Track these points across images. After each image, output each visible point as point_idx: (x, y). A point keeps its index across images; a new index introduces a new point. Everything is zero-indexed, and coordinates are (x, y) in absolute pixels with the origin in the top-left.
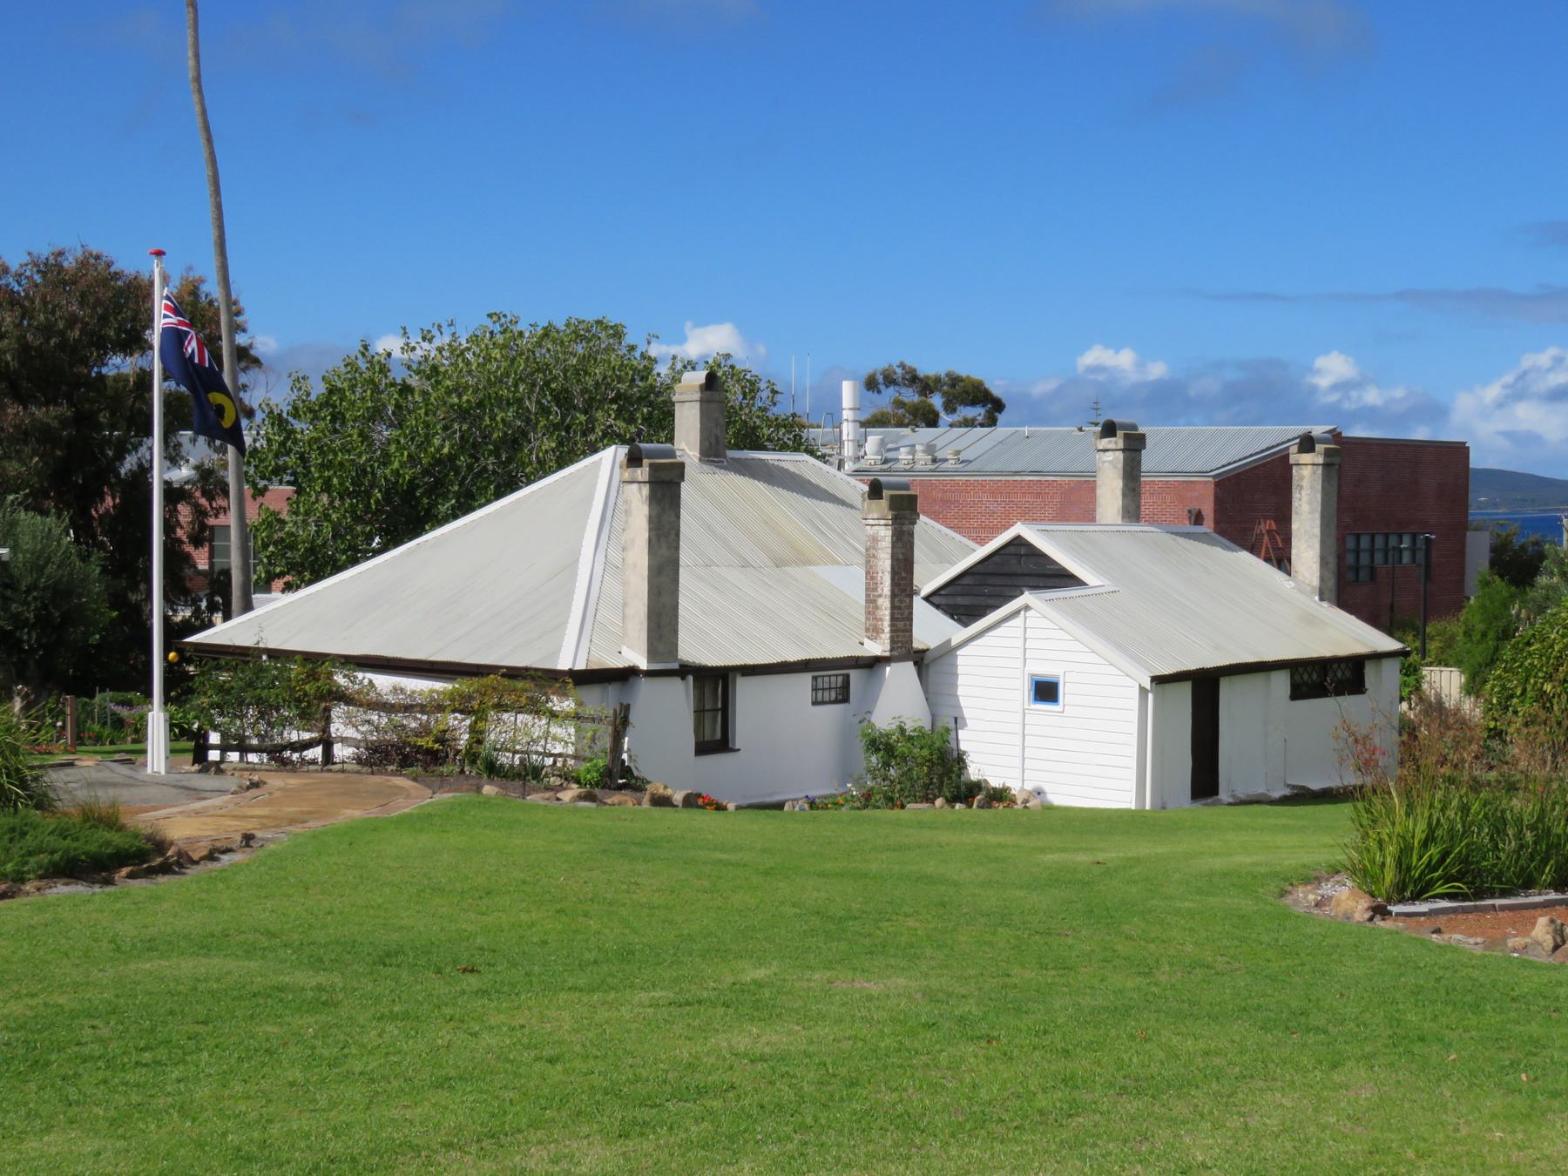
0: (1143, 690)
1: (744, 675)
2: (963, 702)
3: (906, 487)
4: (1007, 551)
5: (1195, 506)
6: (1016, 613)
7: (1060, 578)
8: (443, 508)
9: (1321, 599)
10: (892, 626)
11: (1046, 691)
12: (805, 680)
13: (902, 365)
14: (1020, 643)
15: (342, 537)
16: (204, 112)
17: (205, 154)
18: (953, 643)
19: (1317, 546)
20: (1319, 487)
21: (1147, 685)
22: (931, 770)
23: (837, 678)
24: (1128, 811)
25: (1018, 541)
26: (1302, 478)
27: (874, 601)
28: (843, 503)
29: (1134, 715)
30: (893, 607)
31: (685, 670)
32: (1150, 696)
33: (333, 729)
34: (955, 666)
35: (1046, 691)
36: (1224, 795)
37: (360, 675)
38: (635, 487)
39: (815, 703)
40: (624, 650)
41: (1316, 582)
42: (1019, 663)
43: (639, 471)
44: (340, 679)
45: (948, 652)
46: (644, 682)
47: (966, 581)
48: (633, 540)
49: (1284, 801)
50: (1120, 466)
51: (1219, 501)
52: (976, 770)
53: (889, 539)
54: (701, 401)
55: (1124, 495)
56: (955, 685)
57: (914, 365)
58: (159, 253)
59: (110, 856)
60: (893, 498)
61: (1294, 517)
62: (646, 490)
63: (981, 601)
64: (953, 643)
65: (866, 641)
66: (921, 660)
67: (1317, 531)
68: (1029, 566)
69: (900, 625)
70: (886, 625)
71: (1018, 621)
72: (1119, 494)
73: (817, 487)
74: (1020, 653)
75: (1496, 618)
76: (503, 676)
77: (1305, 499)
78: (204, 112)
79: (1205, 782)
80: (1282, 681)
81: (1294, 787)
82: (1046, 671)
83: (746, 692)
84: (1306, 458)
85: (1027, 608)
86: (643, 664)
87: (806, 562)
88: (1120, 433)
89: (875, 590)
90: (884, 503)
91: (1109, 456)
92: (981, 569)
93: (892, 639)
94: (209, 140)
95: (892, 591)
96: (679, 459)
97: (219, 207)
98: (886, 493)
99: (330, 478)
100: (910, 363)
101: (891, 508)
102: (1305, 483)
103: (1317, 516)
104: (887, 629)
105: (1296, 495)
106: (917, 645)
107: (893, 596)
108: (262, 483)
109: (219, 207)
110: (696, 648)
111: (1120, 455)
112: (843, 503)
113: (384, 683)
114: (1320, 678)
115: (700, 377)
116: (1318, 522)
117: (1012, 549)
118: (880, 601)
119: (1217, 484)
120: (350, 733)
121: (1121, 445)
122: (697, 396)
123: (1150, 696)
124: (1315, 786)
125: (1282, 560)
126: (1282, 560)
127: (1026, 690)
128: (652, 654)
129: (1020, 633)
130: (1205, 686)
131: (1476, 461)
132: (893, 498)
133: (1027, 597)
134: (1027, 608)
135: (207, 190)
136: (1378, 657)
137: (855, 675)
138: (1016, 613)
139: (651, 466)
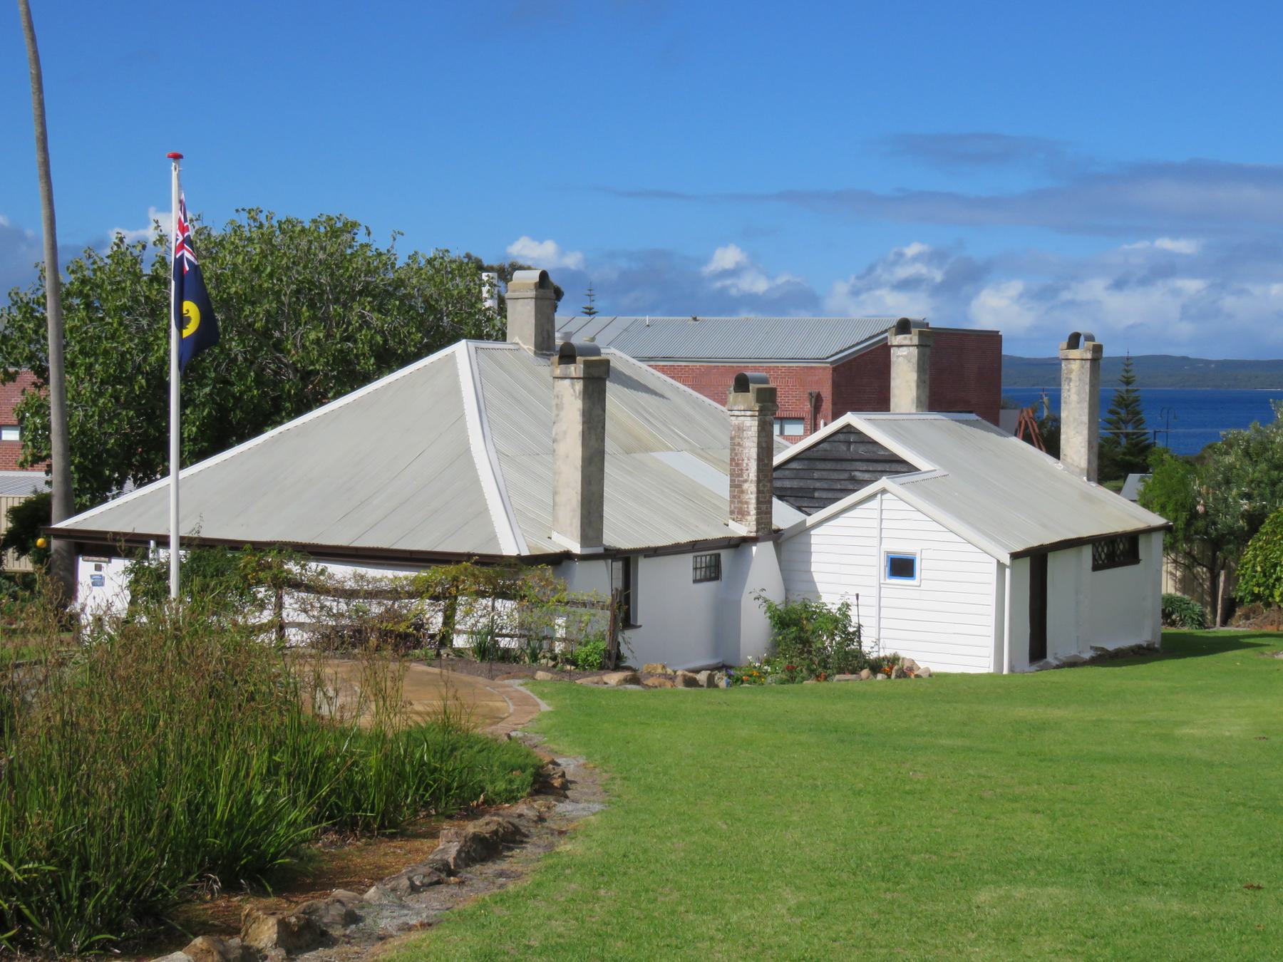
0: (1001, 566)
1: (646, 556)
2: (816, 577)
3: (765, 381)
4: (836, 438)
5: (815, 390)
6: (872, 497)
7: (895, 465)
8: (330, 395)
9: (1089, 480)
10: (758, 508)
11: (902, 567)
12: (688, 560)
13: (468, 256)
14: (876, 523)
15: (110, 421)
16: (28, 13)
17: (28, 54)
18: (808, 524)
19: (1086, 432)
20: (1087, 380)
21: (1006, 560)
22: (812, 643)
23: (715, 559)
24: (989, 675)
25: (848, 429)
26: (1071, 371)
27: (739, 486)
28: (656, 394)
29: (992, 589)
30: (759, 492)
31: (611, 554)
32: (1008, 571)
33: (284, 615)
34: (809, 544)
35: (902, 567)
36: (1050, 658)
37: (313, 565)
38: (567, 382)
39: (695, 581)
40: (555, 536)
41: (1084, 463)
42: (876, 542)
43: (572, 367)
44: (293, 567)
45: (802, 532)
46: (578, 565)
47: (794, 465)
48: (565, 433)
49: (1094, 662)
50: (915, 360)
51: (836, 386)
52: (870, 646)
53: (755, 429)
54: (536, 298)
55: (918, 387)
56: (809, 563)
57: (480, 257)
58: (177, 157)
59: (396, 770)
60: (759, 391)
61: (1063, 406)
62: (579, 386)
63: (851, 487)
64: (808, 524)
65: (731, 523)
66: (776, 536)
67: (1085, 418)
68: (862, 450)
69: (764, 507)
70: (752, 508)
71: (874, 504)
72: (913, 385)
73: (630, 378)
74: (876, 533)
75: (1174, 492)
76: (476, 563)
77: (1073, 390)
78: (28, 13)
79: (1038, 650)
80: (1087, 552)
81: (1096, 649)
82: (902, 548)
83: (645, 568)
84: (1074, 354)
85: (884, 491)
86: (576, 549)
87: (648, 449)
88: (915, 331)
89: (740, 475)
90: (751, 396)
91: (904, 351)
92: (803, 456)
93: (757, 520)
94: (33, 39)
95: (758, 477)
96: (603, 357)
97: (41, 104)
98: (751, 386)
99: (91, 365)
100: (474, 254)
101: (758, 400)
102: (1073, 376)
103: (1086, 405)
104: (753, 512)
105: (1065, 387)
106: (774, 527)
107: (759, 481)
108: (12, 370)
109: (41, 104)
110: (617, 535)
111: (915, 351)
112: (656, 394)
113: (341, 572)
114: (1116, 550)
115: (534, 276)
116: (1086, 411)
117: (841, 437)
118: (746, 486)
119: (834, 370)
120: (303, 618)
121: (916, 341)
122: (533, 293)
123: (1008, 571)
124: (1111, 647)
125: (1051, 445)
126: (1051, 445)
127: (882, 565)
128: (585, 540)
129: (876, 514)
130: (1036, 561)
131: (1006, 350)
132: (759, 391)
133: (884, 482)
134: (884, 491)
135: (31, 87)
136: (1150, 531)
137: (725, 555)
138: (872, 497)
139: (586, 363)
